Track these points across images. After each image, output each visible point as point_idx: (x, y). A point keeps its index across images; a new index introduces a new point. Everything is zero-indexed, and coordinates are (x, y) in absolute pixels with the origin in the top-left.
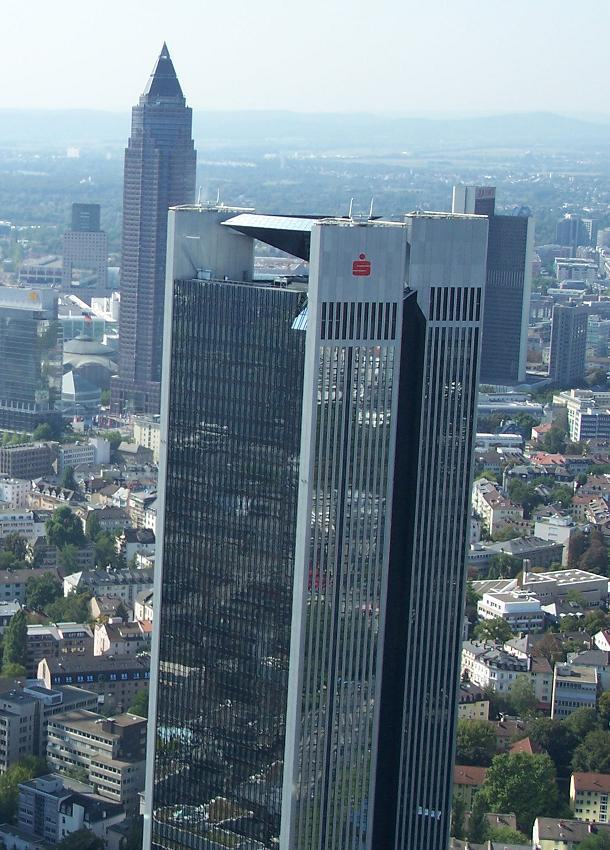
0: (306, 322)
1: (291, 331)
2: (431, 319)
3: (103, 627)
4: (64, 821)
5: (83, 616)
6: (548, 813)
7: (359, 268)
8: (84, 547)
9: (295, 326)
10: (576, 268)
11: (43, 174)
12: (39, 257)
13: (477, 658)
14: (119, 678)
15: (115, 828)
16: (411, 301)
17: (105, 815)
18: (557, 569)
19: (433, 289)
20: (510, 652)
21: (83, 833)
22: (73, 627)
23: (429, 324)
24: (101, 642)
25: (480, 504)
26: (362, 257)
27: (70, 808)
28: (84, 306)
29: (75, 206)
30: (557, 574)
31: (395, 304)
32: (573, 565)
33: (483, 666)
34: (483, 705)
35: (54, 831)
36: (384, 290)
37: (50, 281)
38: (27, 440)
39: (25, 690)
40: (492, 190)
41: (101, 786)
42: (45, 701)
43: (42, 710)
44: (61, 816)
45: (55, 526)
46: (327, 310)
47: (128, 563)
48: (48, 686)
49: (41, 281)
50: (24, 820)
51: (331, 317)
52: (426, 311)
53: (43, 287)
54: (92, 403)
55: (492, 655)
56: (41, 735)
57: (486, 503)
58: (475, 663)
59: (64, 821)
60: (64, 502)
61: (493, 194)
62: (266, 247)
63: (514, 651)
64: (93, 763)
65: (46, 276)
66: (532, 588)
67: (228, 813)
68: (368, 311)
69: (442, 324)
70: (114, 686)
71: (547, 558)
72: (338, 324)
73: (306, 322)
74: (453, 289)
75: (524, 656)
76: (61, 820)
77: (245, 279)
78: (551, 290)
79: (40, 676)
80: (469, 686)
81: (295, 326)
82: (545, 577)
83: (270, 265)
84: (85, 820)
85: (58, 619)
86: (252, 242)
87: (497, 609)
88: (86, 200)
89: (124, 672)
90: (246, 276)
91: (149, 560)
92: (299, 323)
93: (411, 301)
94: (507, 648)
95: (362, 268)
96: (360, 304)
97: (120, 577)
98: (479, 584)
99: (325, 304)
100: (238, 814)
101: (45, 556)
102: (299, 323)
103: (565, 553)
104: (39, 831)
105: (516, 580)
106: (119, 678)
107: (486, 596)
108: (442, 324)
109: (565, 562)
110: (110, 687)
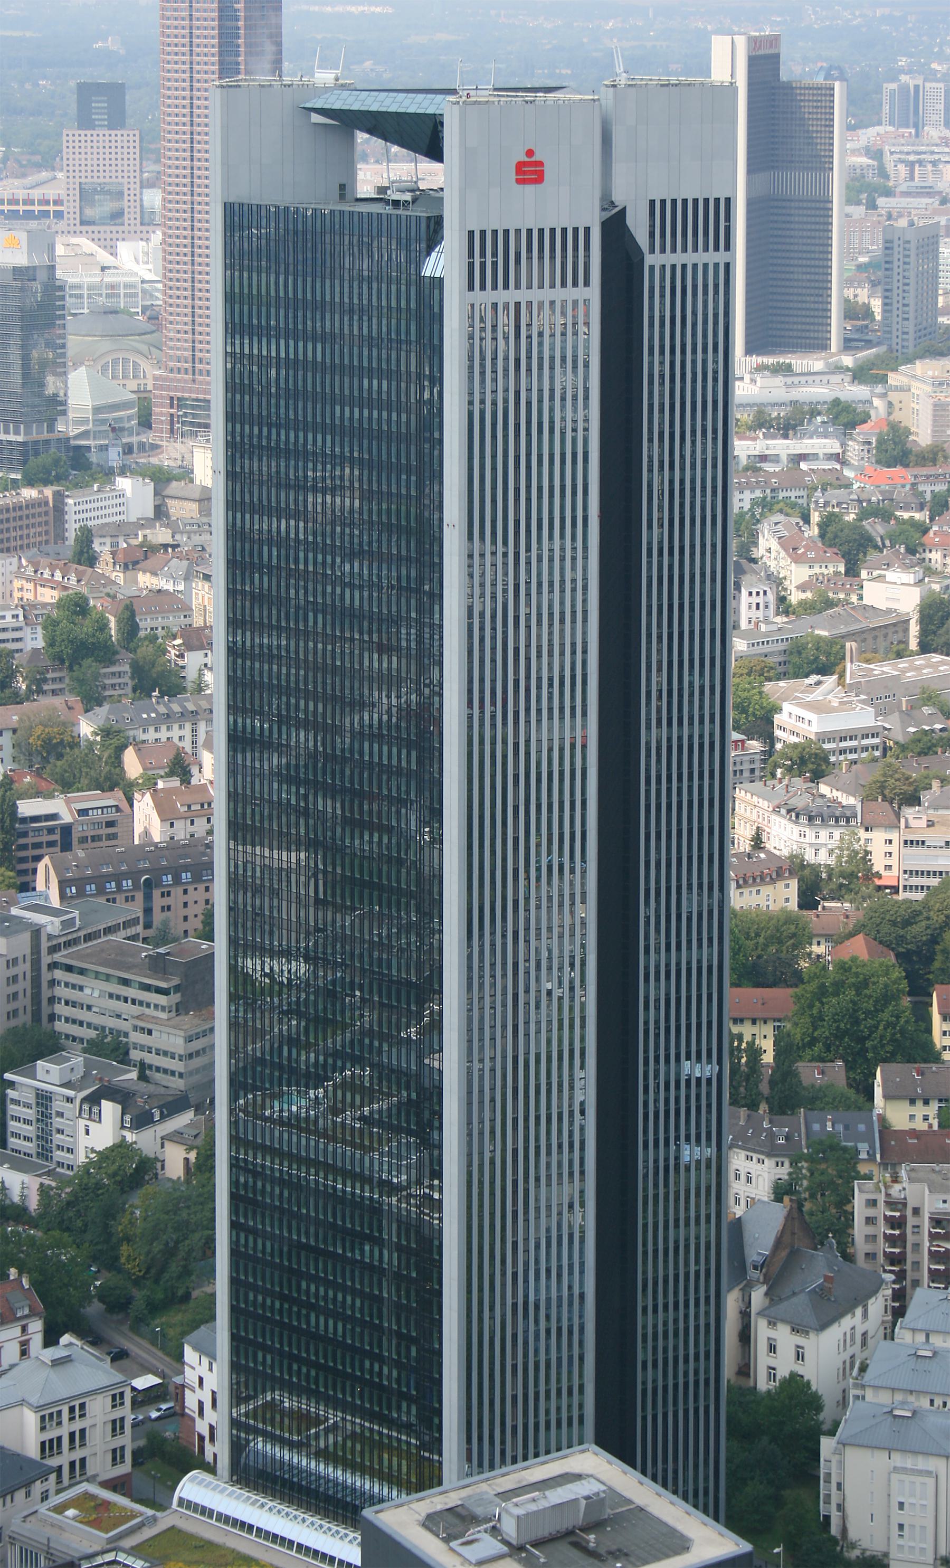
0: (444, 263)
1: (420, 279)
2: (652, 251)
3: (148, 795)
4: (87, 1133)
5: (113, 780)
6: (899, 1057)
7: (525, 173)
8: (113, 663)
9: (427, 271)
10: (920, 162)
11: (28, 34)
12: (24, 176)
13: (776, 810)
14: (177, 881)
15: (176, 1137)
16: (615, 225)
17: (157, 1118)
18: (899, 655)
19: (652, 202)
20: (829, 795)
21: (121, 1147)
22: (95, 800)
23: (649, 260)
24: (146, 820)
25: (773, 555)
26: (530, 153)
27: (95, 1109)
28: (104, 257)
29: (81, 87)
30: (903, 664)
31: (587, 230)
32: (925, 648)
33: (784, 822)
34: (787, 886)
35: (70, 1150)
36: (568, 203)
37: (45, 214)
38: (15, 484)
39: (14, 911)
40: (774, 40)
41: (150, 1067)
42: (49, 929)
43: (45, 945)
44: (82, 1123)
45: (58, 629)
46: (475, 241)
47: (189, 685)
48: (55, 902)
49: (29, 215)
50: (18, 1136)
51: (483, 254)
52: (642, 239)
53: (33, 224)
54: (120, 419)
55: (801, 801)
56: (44, 1003)
57: (783, 554)
58: (774, 817)
59: (87, 1133)
60: (761, 1240)
61: (777, 46)
62: (377, 143)
63: (836, 794)
64: (135, 1028)
65: (36, 208)
66: (856, 688)
67: (369, 1095)
68: (544, 242)
69: (669, 259)
70: (169, 894)
71: (885, 638)
72: (495, 264)
73: (444, 263)
74: (717, 200)
75: (851, 801)
76: (82, 1130)
77: (342, 197)
78: (881, 201)
79: (40, 885)
80: (762, 856)
81: (427, 271)
82: (885, 669)
83: (381, 170)
84: (123, 1127)
85: (66, 785)
86: (352, 138)
87: (805, 726)
88: (103, 76)
89: (186, 868)
90: (344, 190)
91: (209, 671)
92: (433, 266)
93: (615, 225)
94: (824, 789)
95: (530, 172)
96: (564, 231)
97: (176, 708)
98: (775, 688)
99: (471, 234)
100: (390, 1095)
101: (45, 680)
102: (433, 266)
103: (914, 629)
104: (45, 1153)
105: (835, 677)
106: (177, 881)
107: (787, 707)
108: (669, 259)
109: (913, 645)
110: (163, 895)
